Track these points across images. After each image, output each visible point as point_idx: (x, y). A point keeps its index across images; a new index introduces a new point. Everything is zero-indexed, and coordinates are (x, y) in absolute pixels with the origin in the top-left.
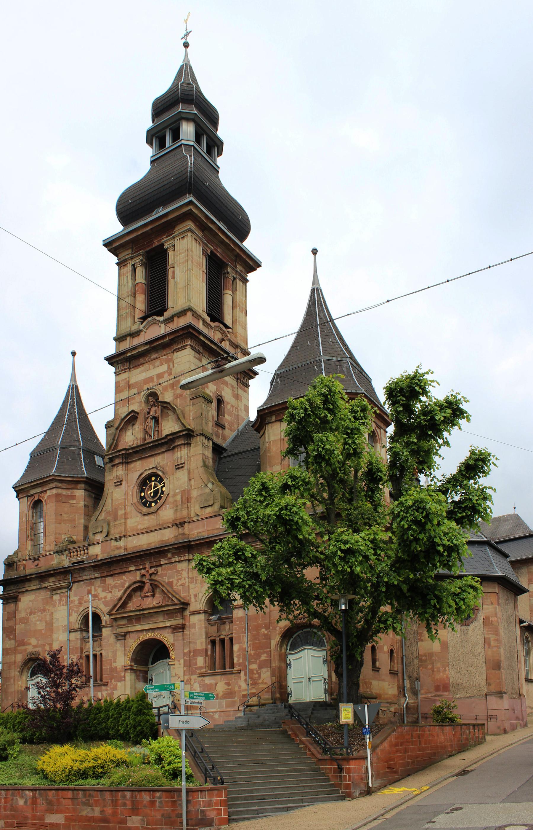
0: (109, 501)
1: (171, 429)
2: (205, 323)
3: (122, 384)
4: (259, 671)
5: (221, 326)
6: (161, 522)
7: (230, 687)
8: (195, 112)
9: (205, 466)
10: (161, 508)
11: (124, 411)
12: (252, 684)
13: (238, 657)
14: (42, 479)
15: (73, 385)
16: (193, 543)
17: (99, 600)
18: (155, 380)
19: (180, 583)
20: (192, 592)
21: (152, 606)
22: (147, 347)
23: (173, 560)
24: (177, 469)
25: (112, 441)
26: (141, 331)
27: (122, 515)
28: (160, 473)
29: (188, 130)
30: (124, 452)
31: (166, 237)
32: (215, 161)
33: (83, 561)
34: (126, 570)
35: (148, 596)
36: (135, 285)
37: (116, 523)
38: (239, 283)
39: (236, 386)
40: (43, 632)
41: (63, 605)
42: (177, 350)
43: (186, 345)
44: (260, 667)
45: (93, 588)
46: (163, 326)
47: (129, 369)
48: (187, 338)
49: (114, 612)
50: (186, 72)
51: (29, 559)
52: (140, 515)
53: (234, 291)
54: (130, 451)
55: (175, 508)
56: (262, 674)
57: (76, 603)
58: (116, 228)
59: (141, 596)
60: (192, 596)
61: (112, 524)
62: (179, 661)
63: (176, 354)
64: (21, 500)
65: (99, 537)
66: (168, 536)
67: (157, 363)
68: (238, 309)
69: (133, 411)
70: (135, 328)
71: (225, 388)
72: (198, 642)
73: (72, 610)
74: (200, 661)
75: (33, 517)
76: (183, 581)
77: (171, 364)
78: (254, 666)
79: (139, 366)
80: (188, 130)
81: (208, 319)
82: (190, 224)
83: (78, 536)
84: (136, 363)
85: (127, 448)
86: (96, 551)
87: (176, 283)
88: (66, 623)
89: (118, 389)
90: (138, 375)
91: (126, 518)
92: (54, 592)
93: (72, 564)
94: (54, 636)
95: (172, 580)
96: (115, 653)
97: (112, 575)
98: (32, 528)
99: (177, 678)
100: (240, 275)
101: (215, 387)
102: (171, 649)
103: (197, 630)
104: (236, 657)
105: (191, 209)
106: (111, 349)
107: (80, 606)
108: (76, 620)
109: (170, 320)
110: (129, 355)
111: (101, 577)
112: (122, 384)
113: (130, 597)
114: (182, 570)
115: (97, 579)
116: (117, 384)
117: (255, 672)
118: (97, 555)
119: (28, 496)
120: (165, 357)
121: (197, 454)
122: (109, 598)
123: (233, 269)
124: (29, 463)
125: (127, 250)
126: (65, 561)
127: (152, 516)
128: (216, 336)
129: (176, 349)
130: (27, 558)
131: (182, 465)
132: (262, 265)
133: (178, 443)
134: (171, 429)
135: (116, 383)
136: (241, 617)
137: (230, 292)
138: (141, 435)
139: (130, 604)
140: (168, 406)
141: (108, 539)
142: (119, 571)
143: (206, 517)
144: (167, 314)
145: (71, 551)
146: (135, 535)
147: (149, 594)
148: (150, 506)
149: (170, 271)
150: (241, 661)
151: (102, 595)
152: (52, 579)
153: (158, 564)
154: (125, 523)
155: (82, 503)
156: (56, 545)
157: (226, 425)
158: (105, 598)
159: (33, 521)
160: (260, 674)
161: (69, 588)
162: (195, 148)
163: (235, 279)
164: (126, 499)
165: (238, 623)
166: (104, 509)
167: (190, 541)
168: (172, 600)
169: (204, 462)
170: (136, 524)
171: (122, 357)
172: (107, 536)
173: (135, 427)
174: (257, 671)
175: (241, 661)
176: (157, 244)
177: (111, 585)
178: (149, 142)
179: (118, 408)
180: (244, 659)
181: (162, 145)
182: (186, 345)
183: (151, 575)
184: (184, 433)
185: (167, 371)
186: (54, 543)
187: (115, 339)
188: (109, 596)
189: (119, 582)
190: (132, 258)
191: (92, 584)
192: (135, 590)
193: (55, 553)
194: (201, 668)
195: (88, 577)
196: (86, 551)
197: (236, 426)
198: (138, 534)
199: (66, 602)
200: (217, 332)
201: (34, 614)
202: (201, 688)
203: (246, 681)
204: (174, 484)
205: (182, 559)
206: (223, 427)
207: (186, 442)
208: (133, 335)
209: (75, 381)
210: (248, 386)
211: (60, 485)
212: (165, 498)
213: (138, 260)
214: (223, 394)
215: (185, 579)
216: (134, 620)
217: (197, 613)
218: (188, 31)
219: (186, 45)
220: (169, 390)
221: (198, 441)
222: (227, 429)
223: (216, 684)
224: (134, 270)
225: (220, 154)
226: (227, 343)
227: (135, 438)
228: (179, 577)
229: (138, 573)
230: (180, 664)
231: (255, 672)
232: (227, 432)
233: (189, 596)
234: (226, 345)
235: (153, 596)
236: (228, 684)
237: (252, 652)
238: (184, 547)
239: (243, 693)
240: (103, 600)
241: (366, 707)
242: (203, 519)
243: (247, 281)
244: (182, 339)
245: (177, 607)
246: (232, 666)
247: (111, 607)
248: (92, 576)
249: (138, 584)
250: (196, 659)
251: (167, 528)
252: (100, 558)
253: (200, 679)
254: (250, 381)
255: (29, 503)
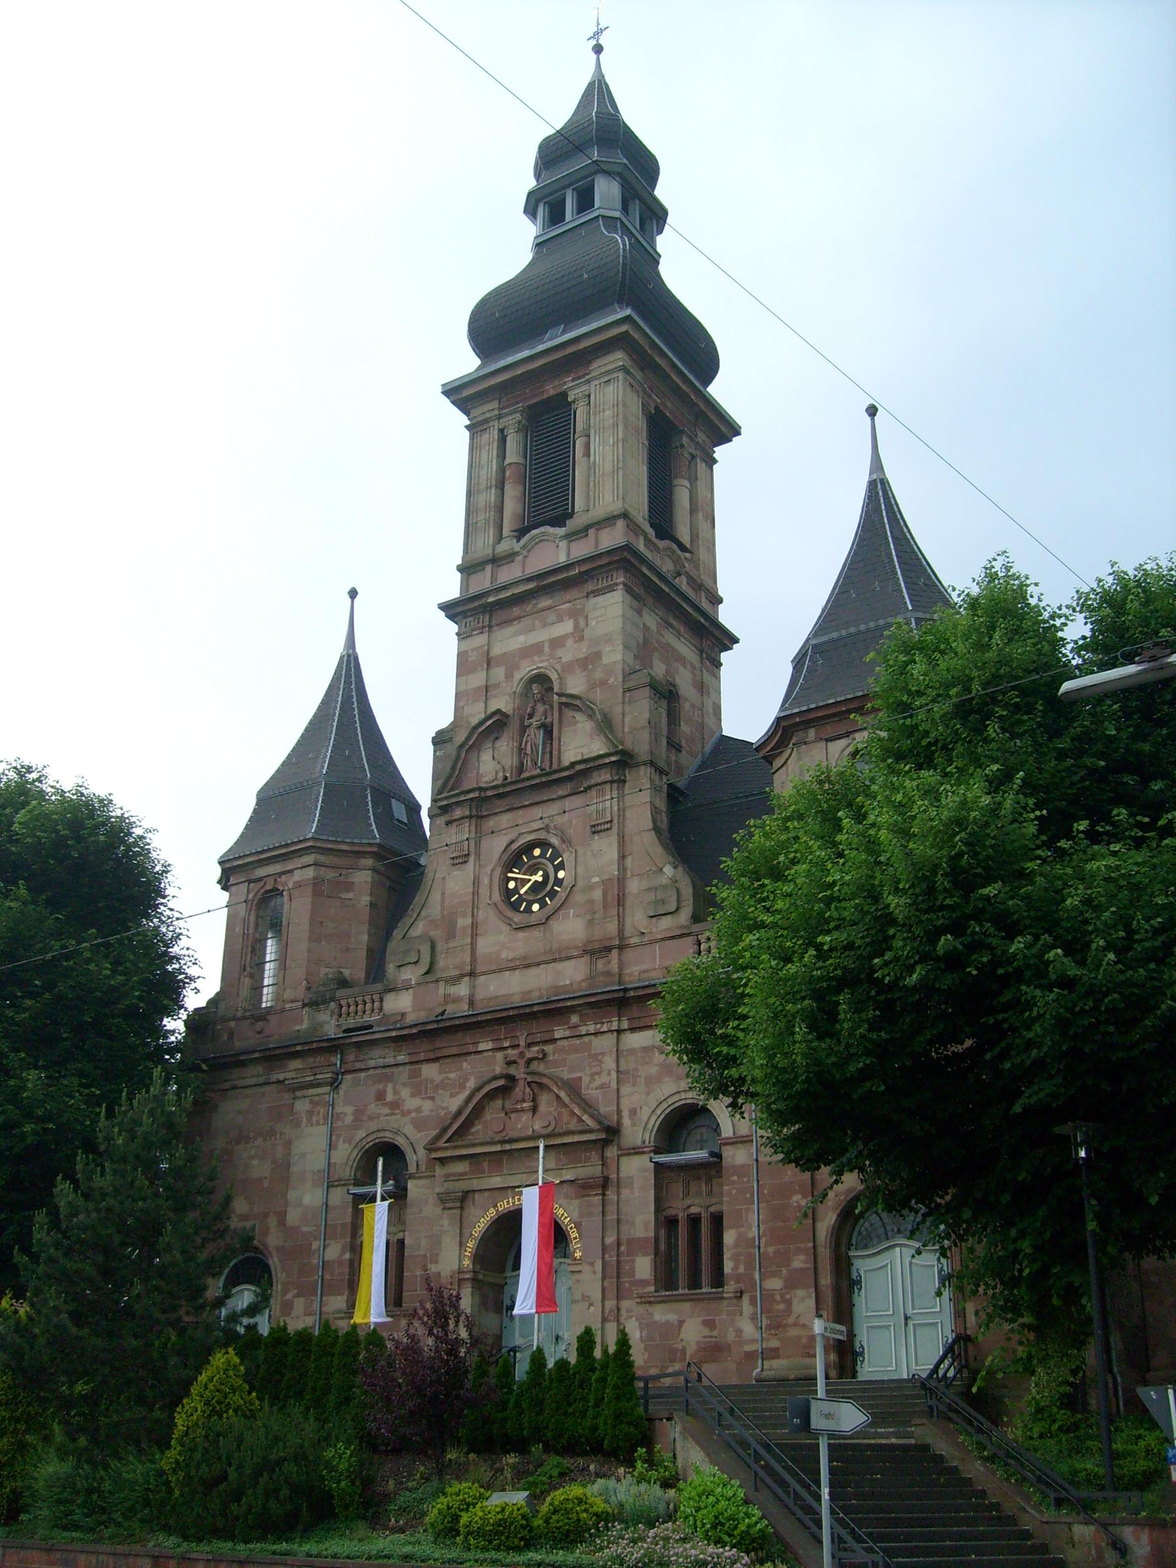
0: (436, 896)
1: (580, 750)
2: (648, 542)
3: (473, 657)
4: (788, 1297)
5: (675, 546)
6: (555, 946)
7: (715, 1333)
8: (625, 161)
9: (656, 829)
10: (556, 915)
11: (477, 712)
12: (769, 1327)
13: (736, 1258)
14: (287, 845)
15: (349, 656)
16: (632, 994)
17: (403, 1114)
18: (547, 650)
19: (598, 1083)
20: (626, 1104)
21: (530, 1132)
22: (532, 585)
23: (583, 1030)
24: (594, 833)
25: (449, 770)
26: (516, 554)
27: (464, 928)
28: (554, 841)
29: (607, 192)
30: (476, 794)
31: (573, 380)
32: (653, 245)
33: (371, 1027)
34: (472, 1048)
35: (522, 1110)
36: (502, 470)
37: (451, 945)
38: (701, 466)
39: (698, 665)
40: (266, 1183)
41: (318, 1124)
42: (596, 593)
43: (616, 584)
44: (792, 1283)
45: (390, 1087)
46: (563, 544)
47: (490, 627)
48: (618, 569)
49: (441, 1144)
50: (598, 92)
51: (244, 1018)
52: (506, 928)
53: (693, 479)
54: (490, 793)
55: (588, 917)
56: (795, 1303)
57: (349, 1119)
58: (467, 363)
59: (503, 1108)
60: (625, 1114)
61: (440, 946)
62: (592, 1264)
63: (593, 601)
64: (233, 889)
65: (410, 975)
66: (572, 975)
67: (552, 617)
68: (700, 514)
69: (499, 711)
70: (504, 547)
71: (681, 669)
72: (639, 1220)
73: (338, 1136)
74: (643, 1267)
75: (257, 925)
76: (604, 1079)
77: (582, 622)
78: (775, 1284)
79: (509, 622)
80: (607, 192)
81: (651, 532)
82: (618, 358)
83: (356, 970)
84: (501, 615)
85: (484, 785)
86: (401, 1003)
87: (591, 468)
88: (321, 1164)
89: (464, 666)
90: (509, 640)
91: (474, 936)
92: (298, 1093)
93: (345, 1031)
94: (292, 1195)
95: (580, 1074)
96: (436, 1241)
97: (437, 1059)
98: (253, 951)
99: (586, 1304)
100: (703, 450)
101: (664, 667)
102: (573, 1236)
103: (636, 1191)
104: (730, 1259)
105: (627, 332)
106: (452, 590)
107: (357, 1128)
108: (346, 1155)
109: (584, 531)
110: (491, 599)
111: (411, 1063)
112: (473, 657)
113: (478, 1111)
114: (603, 1054)
115: (401, 1068)
116: (462, 658)
117: (778, 1298)
118: (403, 1014)
119: (250, 881)
120: (568, 605)
121: (639, 804)
122: (426, 1112)
123: (692, 440)
124: (255, 811)
125: (488, 402)
126: (330, 1025)
127: (536, 933)
128: (667, 567)
129: (593, 592)
130: (239, 1014)
131: (606, 826)
132: (742, 431)
133: (597, 777)
134: (580, 750)
135: (459, 655)
136: (743, 1166)
137: (687, 483)
138: (510, 761)
139: (478, 1127)
140: (578, 702)
141: (430, 978)
142: (454, 1051)
143: (659, 937)
144: (572, 524)
145: (343, 1002)
146: (494, 972)
147: (525, 1105)
148: (528, 910)
149: (579, 443)
150: (742, 1270)
151: (411, 1103)
152: (296, 1064)
153: (546, 1037)
154: (473, 945)
155: (366, 899)
156: (309, 989)
157: (683, 743)
158: (419, 1110)
159: (257, 935)
160: (789, 1303)
161: (335, 1084)
162: (622, 222)
163: (693, 457)
164: (476, 893)
165: (735, 1178)
166: (423, 913)
167: (625, 990)
168: (580, 1120)
169: (654, 821)
170: (497, 948)
171: (476, 604)
172: (426, 973)
173: (498, 744)
174: (782, 1296)
175: (742, 1270)
176: (552, 393)
177: (432, 1081)
178: (530, 210)
179: (461, 704)
180: (750, 1266)
181: (556, 215)
182: (616, 584)
183: (529, 1061)
184: (613, 759)
185: (572, 634)
186: (305, 983)
187: (460, 569)
188: (427, 1106)
189: (452, 1075)
190: (499, 417)
191: (388, 1078)
192: (491, 1095)
193: (304, 1005)
194: (643, 1283)
195: (381, 1062)
196: (377, 1004)
197: (699, 745)
198: (501, 970)
199: (326, 1118)
200: (667, 559)
201: (247, 1143)
202: (645, 1333)
203: (753, 1318)
204: (591, 862)
205: (605, 1028)
206: (678, 748)
207: (616, 778)
208: (495, 561)
209: (354, 648)
210: (719, 665)
211: (322, 859)
212: (564, 895)
213: (512, 421)
214: (678, 681)
215: (609, 1074)
216: (485, 1164)
217: (636, 1151)
218: (602, 26)
219: (598, 49)
220: (578, 671)
221: (643, 777)
222: (684, 752)
223: (681, 1323)
224: (503, 439)
225: (660, 231)
226: (684, 579)
227: (499, 767)
228: (594, 1070)
229: (500, 1055)
230: (594, 1273)
231: (778, 1298)
232: (684, 758)
233: (619, 1112)
234: (682, 583)
235: (534, 1109)
236: (709, 1324)
237: (771, 1249)
238: (609, 1002)
239: (748, 1348)
240: (413, 1115)
241: (1171, 1392)
242: (652, 942)
243: (715, 461)
244: (607, 572)
245: (592, 1137)
246: (718, 1279)
247: (435, 1132)
248: (390, 1060)
249: (502, 1082)
250: (633, 1261)
251: (568, 958)
252: (410, 1020)
253: (641, 1309)
254: (722, 654)
255: (251, 896)
